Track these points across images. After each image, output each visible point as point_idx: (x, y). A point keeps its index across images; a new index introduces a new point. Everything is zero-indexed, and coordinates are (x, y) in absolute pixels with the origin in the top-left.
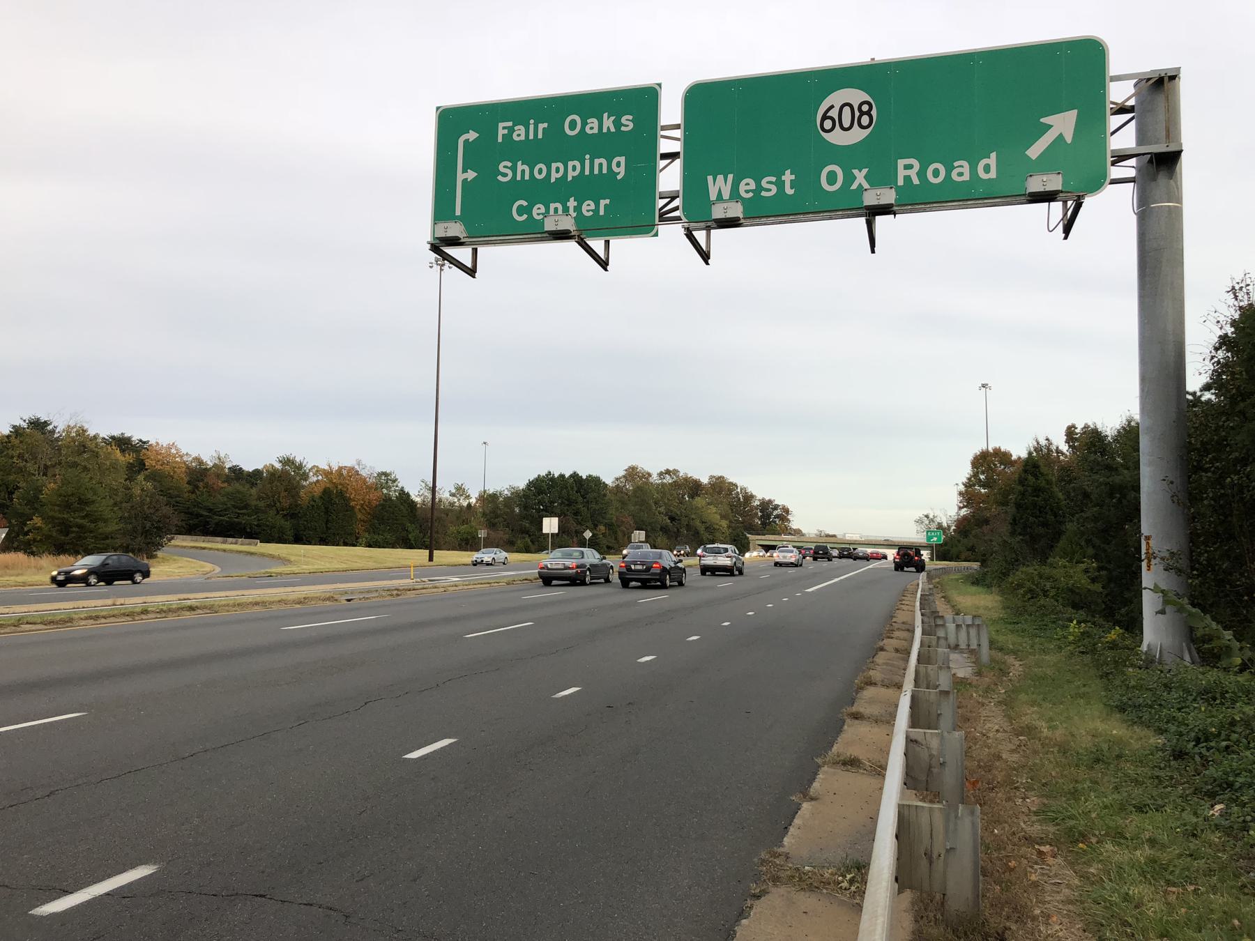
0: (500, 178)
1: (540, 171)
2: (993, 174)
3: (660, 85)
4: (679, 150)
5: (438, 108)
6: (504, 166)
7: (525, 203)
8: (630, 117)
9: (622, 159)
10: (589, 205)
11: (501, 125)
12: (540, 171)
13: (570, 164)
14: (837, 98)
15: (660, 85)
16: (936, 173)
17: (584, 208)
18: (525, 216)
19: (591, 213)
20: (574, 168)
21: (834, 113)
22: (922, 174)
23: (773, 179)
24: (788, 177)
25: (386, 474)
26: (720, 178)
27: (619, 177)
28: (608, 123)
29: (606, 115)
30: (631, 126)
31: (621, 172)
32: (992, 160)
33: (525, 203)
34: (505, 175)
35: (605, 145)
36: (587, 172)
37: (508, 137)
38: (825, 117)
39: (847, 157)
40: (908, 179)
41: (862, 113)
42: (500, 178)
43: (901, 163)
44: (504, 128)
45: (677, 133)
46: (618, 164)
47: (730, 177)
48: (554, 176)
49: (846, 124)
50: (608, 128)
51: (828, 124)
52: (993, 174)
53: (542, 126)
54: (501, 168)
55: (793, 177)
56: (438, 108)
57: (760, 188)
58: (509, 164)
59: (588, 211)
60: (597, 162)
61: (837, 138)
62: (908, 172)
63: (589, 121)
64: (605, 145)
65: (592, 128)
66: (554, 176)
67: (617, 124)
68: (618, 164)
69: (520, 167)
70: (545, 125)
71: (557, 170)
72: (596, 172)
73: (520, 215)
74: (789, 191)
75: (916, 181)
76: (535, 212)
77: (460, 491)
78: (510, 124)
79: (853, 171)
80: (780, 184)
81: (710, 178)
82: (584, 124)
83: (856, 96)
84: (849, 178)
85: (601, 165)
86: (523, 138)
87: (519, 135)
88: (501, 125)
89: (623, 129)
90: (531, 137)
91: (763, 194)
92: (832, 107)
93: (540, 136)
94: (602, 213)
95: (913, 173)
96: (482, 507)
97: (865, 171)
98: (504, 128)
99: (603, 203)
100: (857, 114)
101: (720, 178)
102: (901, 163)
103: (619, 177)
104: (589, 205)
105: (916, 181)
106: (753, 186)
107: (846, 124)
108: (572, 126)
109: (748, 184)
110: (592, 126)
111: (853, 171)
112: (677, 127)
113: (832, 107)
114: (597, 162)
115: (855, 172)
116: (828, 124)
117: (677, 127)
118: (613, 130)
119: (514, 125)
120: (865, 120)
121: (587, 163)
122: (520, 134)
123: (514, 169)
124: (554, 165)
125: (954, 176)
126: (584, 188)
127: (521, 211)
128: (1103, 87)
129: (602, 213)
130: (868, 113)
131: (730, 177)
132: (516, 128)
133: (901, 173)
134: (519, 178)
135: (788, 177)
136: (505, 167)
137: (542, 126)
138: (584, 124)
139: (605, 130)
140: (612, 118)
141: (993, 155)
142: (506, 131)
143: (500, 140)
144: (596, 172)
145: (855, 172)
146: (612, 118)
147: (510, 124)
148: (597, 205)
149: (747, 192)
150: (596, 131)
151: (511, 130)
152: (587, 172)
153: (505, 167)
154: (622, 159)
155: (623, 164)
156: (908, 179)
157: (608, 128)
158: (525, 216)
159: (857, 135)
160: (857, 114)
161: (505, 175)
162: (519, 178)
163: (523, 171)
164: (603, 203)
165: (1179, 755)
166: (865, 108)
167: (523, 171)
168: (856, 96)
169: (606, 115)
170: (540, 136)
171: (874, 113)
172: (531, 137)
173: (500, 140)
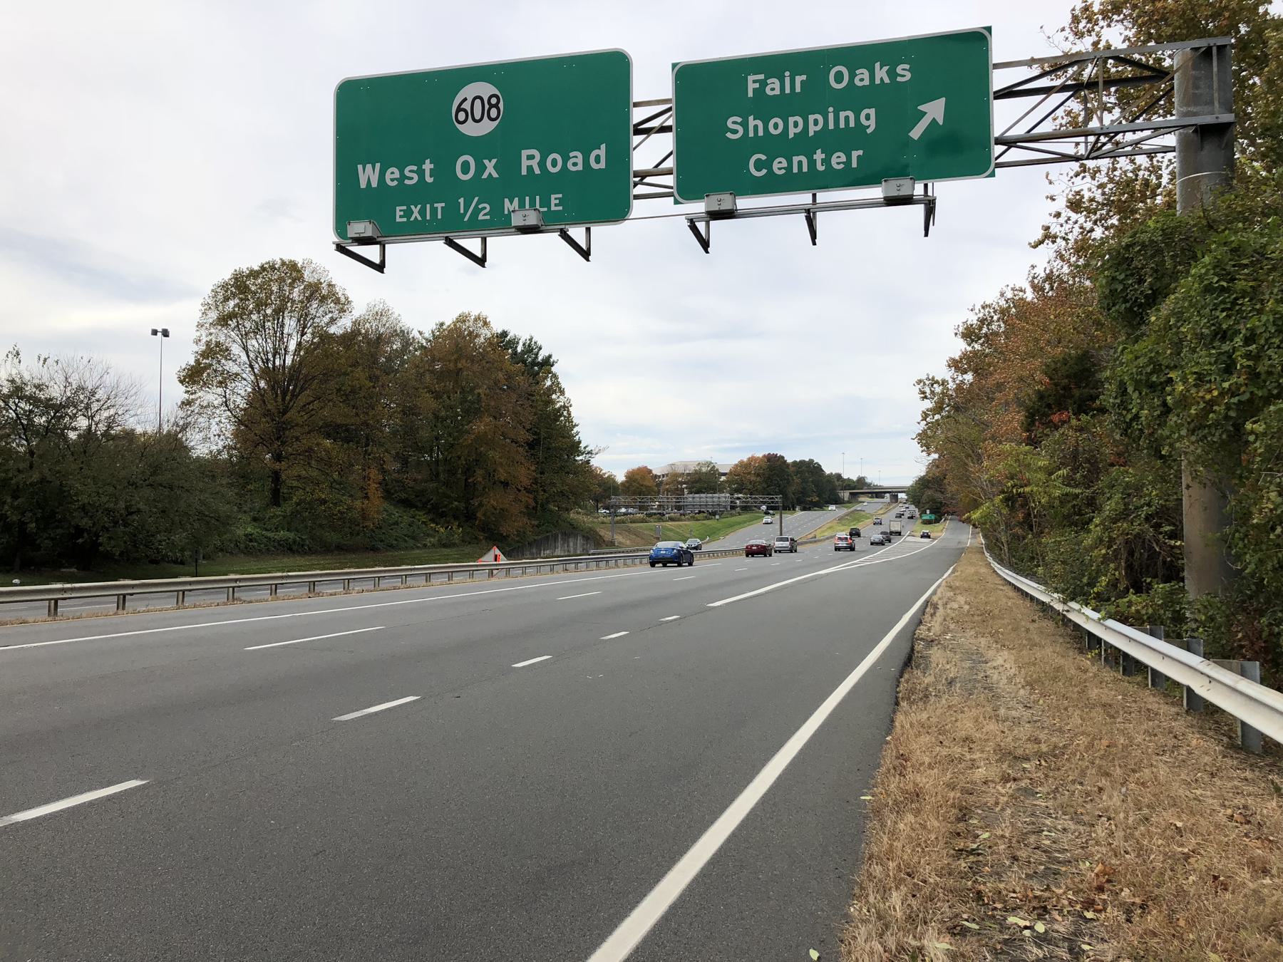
0: (729, 135)
1: (776, 126)
2: (602, 165)
3: (989, 29)
4: (995, 101)
5: (674, 65)
7: (763, 157)
8: (907, 67)
9: (872, 112)
10: (839, 157)
11: (751, 78)
14: (469, 91)
15: (989, 29)
16: (554, 163)
17: (834, 160)
18: (764, 171)
21: (467, 106)
22: (542, 164)
23: (415, 168)
24: (428, 166)
26: (369, 166)
27: (869, 131)
29: (878, 65)
30: (908, 76)
31: (871, 125)
32: (602, 151)
33: (763, 157)
34: (735, 132)
36: (831, 126)
37: (760, 92)
38: (459, 109)
39: (479, 147)
40: (530, 168)
41: (491, 106)
42: (729, 135)
43: (525, 153)
44: (755, 82)
46: (868, 118)
47: (378, 165)
48: (792, 132)
49: (478, 116)
50: (882, 79)
51: (462, 116)
52: (602, 165)
54: (729, 124)
55: (432, 166)
56: (674, 65)
57: (403, 177)
58: (739, 120)
59: (780, 169)
60: (842, 115)
61: (470, 129)
62: (530, 163)
63: (857, 72)
66: (792, 132)
67: (892, 74)
68: (868, 118)
69: (752, 122)
70: (804, 77)
71: (796, 124)
72: (842, 125)
73: (758, 170)
74: (429, 180)
75: (537, 171)
76: (775, 166)
77: (578, 433)
78: (761, 77)
79: (484, 161)
80: (421, 173)
81: (360, 167)
82: (852, 76)
83: (486, 89)
84: (481, 168)
85: (847, 118)
86: (777, 92)
87: (773, 89)
89: (899, 79)
91: (407, 182)
92: (465, 99)
93: (798, 89)
94: (854, 165)
95: (534, 163)
97: (494, 161)
98: (755, 82)
99: (855, 154)
100: (487, 107)
101: (369, 166)
102: (525, 153)
103: (869, 131)
104: (839, 157)
105: (537, 171)
106: (397, 175)
107: (478, 116)
109: (392, 173)
110: (862, 79)
111: (484, 161)
113: (465, 99)
114: (842, 115)
115: (486, 162)
116: (462, 116)
118: (887, 80)
119: (767, 78)
120: (494, 113)
122: (773, 88)
123: (745, 124)
125: (570, 166)
126: (832, 140)
129: (854, 165)
130: (496, 106)
131: (378, 165)
132: (769, 81)
133: (525, 163)
134: (751, 134)
135: (428, 166)
136: (734, 123)
137: (799, 79)
139: (878, 81)
140: (886, 68)
141: (603, 146)
142: (757, 85)
143: (750, 94)
144: (842, 125)
145: (486, 162)
146: (886, 68)
147: (761, 77)
149: (392, 180)
150: (867, 82)
151: (763, 84)
152: (831, 126)
153: (734, 123)
154: (872, 112)
156: (530, 168)
157: (882, 79)
158: (764, 171)
159: (487, 127)
160: (487, 107)
161: (735, 132)
162: (751, 134)
163: (756, 127)
164: (855, 154)
166: (494, 101)
167: (756, 127)
168: (486, 89)
169: (878, 65)
170: (798, 89)
171: (501, 105)
172: (788, 91)
173: (750, 94)
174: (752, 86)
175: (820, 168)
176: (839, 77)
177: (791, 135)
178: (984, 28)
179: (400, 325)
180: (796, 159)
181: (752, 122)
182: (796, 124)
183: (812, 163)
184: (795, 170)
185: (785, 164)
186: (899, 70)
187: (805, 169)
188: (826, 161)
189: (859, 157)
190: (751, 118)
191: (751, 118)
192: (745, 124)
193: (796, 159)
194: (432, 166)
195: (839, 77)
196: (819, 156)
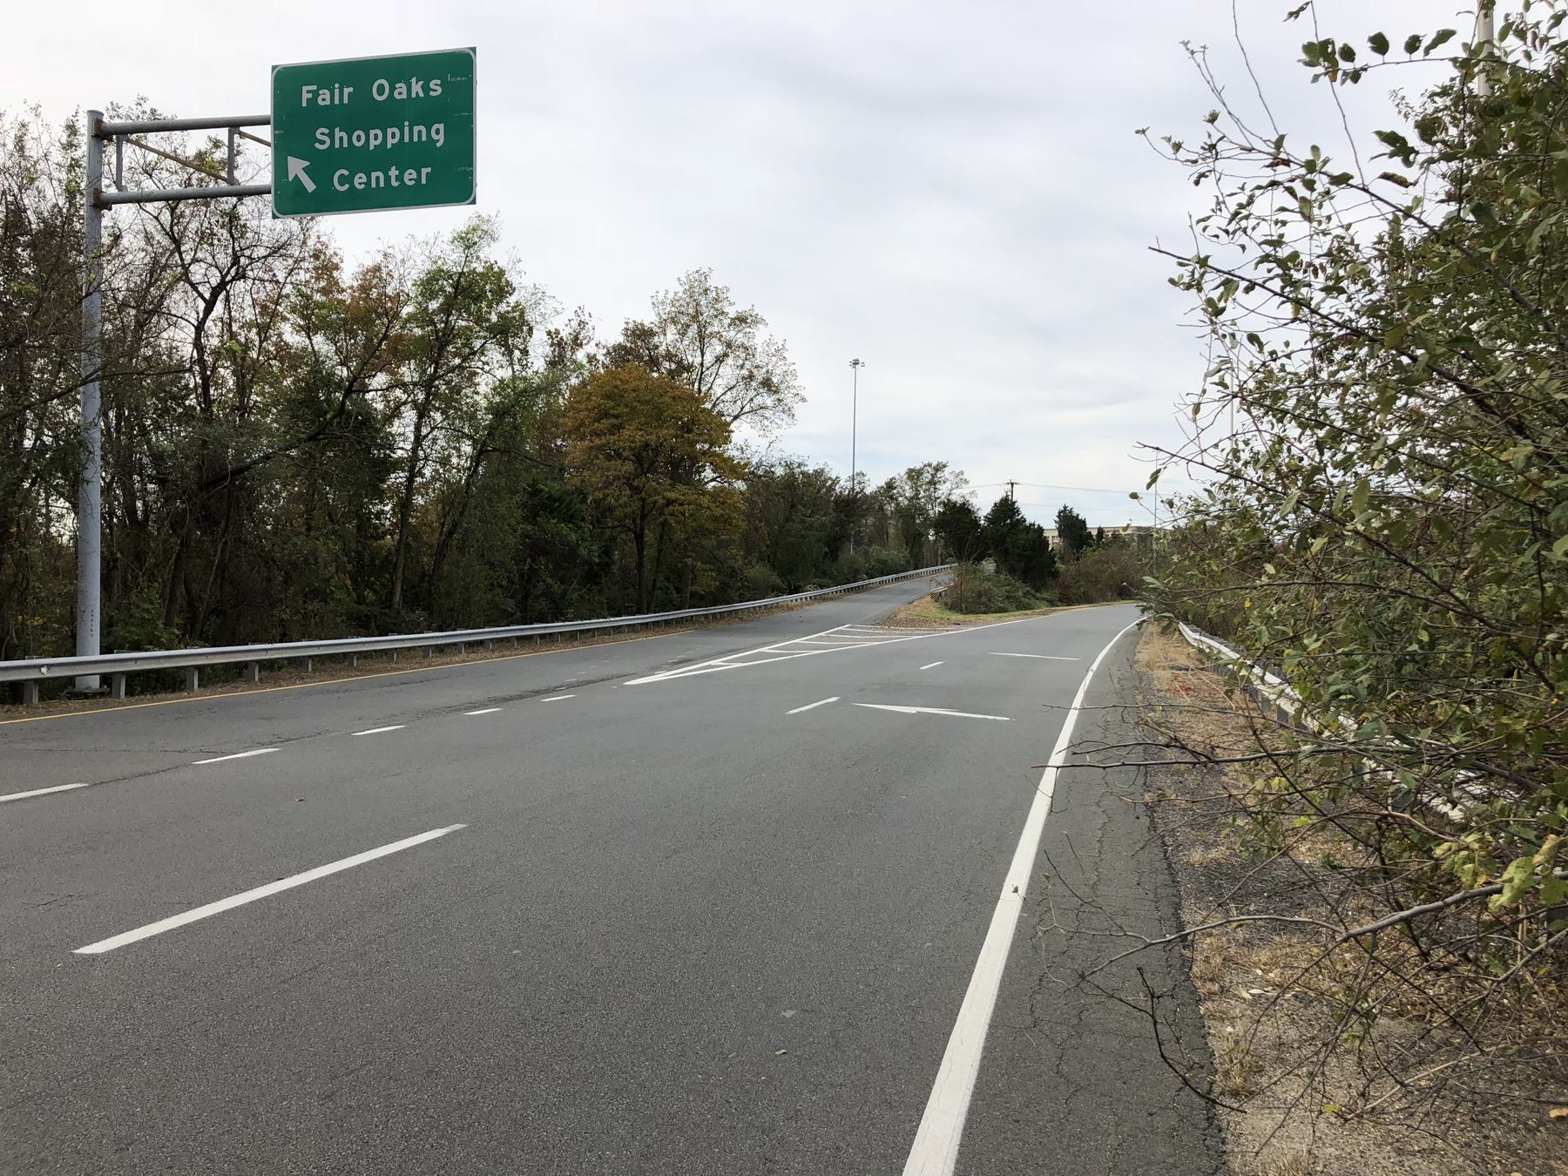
1: (359, 138)
3: (474, 50)
5: (274, 68)
6: (321, 133)
7: (346, 172)
8: (439, 82)
9: (441, 126)
11: (305, 89)
12: (359, 138)
13: (390, 131)
15: (474, 50)
17: (406, 177)
18: (347, 186)
19: (363, 186)
20: (393, 135)
25: (1060, 513)
27: (438, 145)
28: (417, 88)
29: (414, 80)
30: (440, 90)
33: (346, 172)
34: (323, 143)
35: (425, 112)
36: (407, 140)
37: (313, 101)
44: (308, 92)
45: (265, 132)
46: (437, 132)
48: (373, 143)
53: (347, 90)
54: (319, 136)
56: (274, 68)
58: (327, 131)
60: (416, 129)
63: (397, 86)
64: (425, 112)
65: (400, 93)
66: (373, 143)
67: (426, 89)
68: (437, 132)
69: (338, 133)
70: (351, 89)
72: (416, 139)
73: (342, 184)
76: (356, 181)
78: (315, 87)
82: (392, 89)
86: (328, 102)
88: (305, 89)
89: (432, 93)
90: (337, 102)
93: (346, 101)
94: (424, 182)
96: (454, 500)
98: (308, 92)
99: (425, 171)
103: (438, 145)
108: (380, 90)
110: (401, 92)
112: (263, 122)
114: (416, 129)
117: (263, 122)
118: (422, 95)
119: (319, 89)
121: (406, 130)
122: (324, 98)
123: (331, 136)
124: (372, 132)
127: (342, 180)
128: (275, 137)
129: (424, 182)
132: (321, 92)
134: (337, 146)
137: (347, 90)
138: (392, 89)
139: (414, 95)
140: (421, 83)
142: (310, 95)
143: (304, 104)
144: (416, 139)
146: (421, 83)
147: (315, 87)
148: (419, 174)
150: (404, 96)
151: (316, 94)
152: (407, 140)
154: (441, 126)
155: (442, 132)
158: (347, 186)
161: (323, 143)
162: (337, 146)
163: (341, 138)
164: (425, 171)
165: (424, 575)
167: (341, 138)
170: (346, 101)
173: (304, 104)
174: (305, 96)
175: (395, 184)
176: (381, 90)
177: (389, 146)
178: (470, 48)
179: (943, 491)
180: (374, 175)
181: (338, 133)
182: (376, 137)
183: (388, 179)
184: (374, 185)
185: (414, 176)
186: (432, 85)
187: (382, 185)
188: (400, 178)
189: (427, 173)
190: (337, 130)
191: (337, 130)
192: (331, 136)
193: (374, 175)
194: (397, 173)
195: (381, 90)
196: (393, 172)
